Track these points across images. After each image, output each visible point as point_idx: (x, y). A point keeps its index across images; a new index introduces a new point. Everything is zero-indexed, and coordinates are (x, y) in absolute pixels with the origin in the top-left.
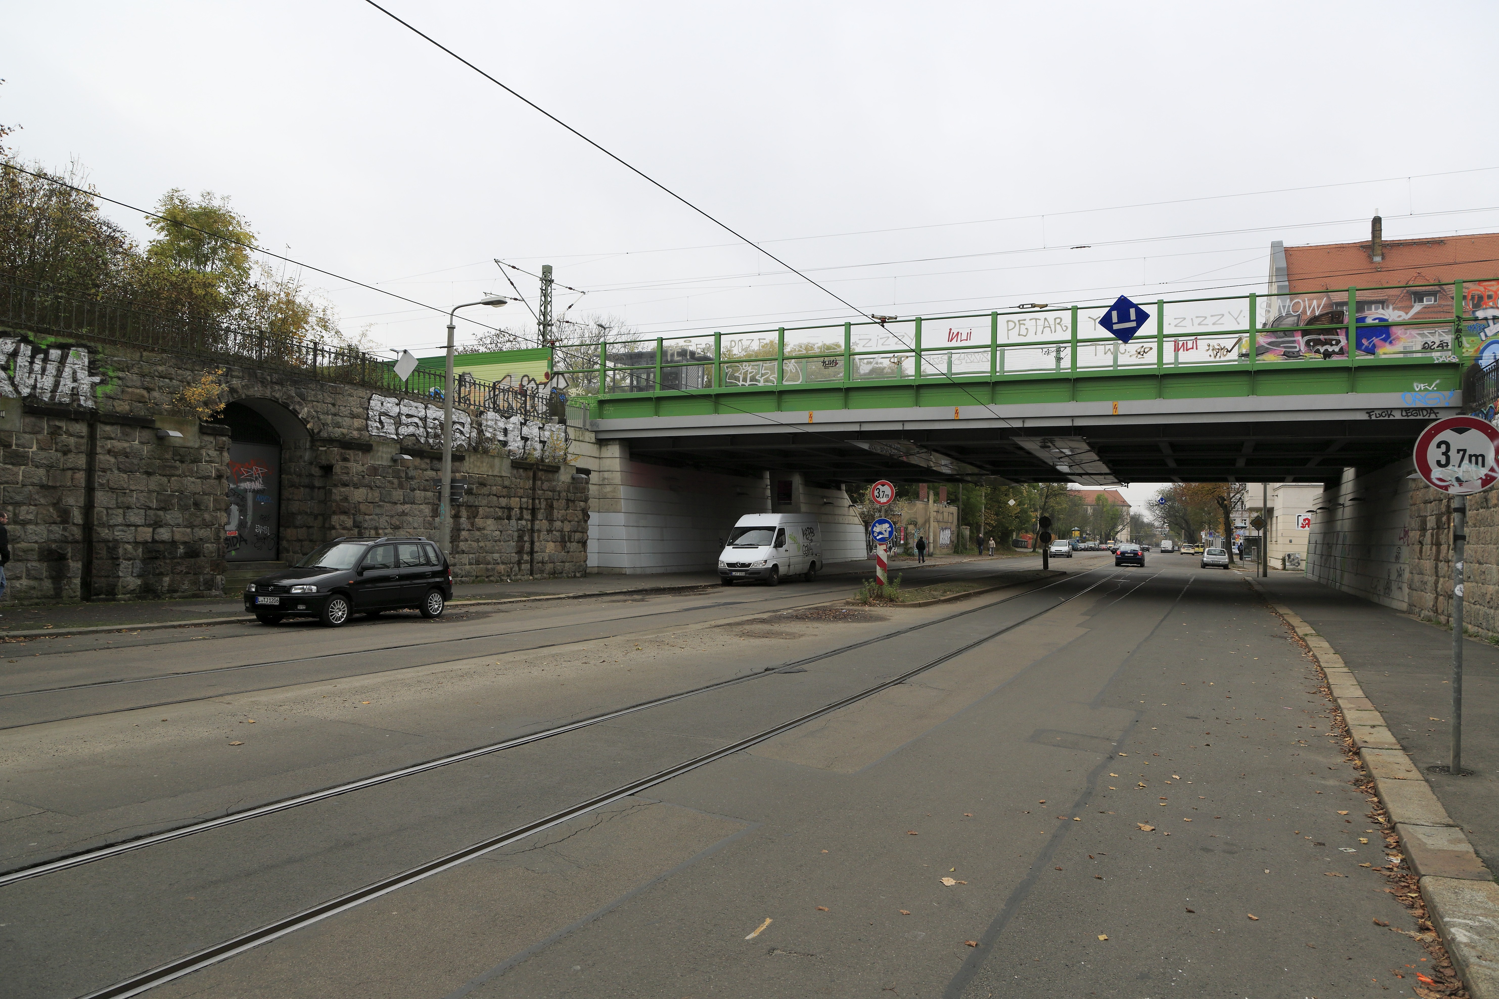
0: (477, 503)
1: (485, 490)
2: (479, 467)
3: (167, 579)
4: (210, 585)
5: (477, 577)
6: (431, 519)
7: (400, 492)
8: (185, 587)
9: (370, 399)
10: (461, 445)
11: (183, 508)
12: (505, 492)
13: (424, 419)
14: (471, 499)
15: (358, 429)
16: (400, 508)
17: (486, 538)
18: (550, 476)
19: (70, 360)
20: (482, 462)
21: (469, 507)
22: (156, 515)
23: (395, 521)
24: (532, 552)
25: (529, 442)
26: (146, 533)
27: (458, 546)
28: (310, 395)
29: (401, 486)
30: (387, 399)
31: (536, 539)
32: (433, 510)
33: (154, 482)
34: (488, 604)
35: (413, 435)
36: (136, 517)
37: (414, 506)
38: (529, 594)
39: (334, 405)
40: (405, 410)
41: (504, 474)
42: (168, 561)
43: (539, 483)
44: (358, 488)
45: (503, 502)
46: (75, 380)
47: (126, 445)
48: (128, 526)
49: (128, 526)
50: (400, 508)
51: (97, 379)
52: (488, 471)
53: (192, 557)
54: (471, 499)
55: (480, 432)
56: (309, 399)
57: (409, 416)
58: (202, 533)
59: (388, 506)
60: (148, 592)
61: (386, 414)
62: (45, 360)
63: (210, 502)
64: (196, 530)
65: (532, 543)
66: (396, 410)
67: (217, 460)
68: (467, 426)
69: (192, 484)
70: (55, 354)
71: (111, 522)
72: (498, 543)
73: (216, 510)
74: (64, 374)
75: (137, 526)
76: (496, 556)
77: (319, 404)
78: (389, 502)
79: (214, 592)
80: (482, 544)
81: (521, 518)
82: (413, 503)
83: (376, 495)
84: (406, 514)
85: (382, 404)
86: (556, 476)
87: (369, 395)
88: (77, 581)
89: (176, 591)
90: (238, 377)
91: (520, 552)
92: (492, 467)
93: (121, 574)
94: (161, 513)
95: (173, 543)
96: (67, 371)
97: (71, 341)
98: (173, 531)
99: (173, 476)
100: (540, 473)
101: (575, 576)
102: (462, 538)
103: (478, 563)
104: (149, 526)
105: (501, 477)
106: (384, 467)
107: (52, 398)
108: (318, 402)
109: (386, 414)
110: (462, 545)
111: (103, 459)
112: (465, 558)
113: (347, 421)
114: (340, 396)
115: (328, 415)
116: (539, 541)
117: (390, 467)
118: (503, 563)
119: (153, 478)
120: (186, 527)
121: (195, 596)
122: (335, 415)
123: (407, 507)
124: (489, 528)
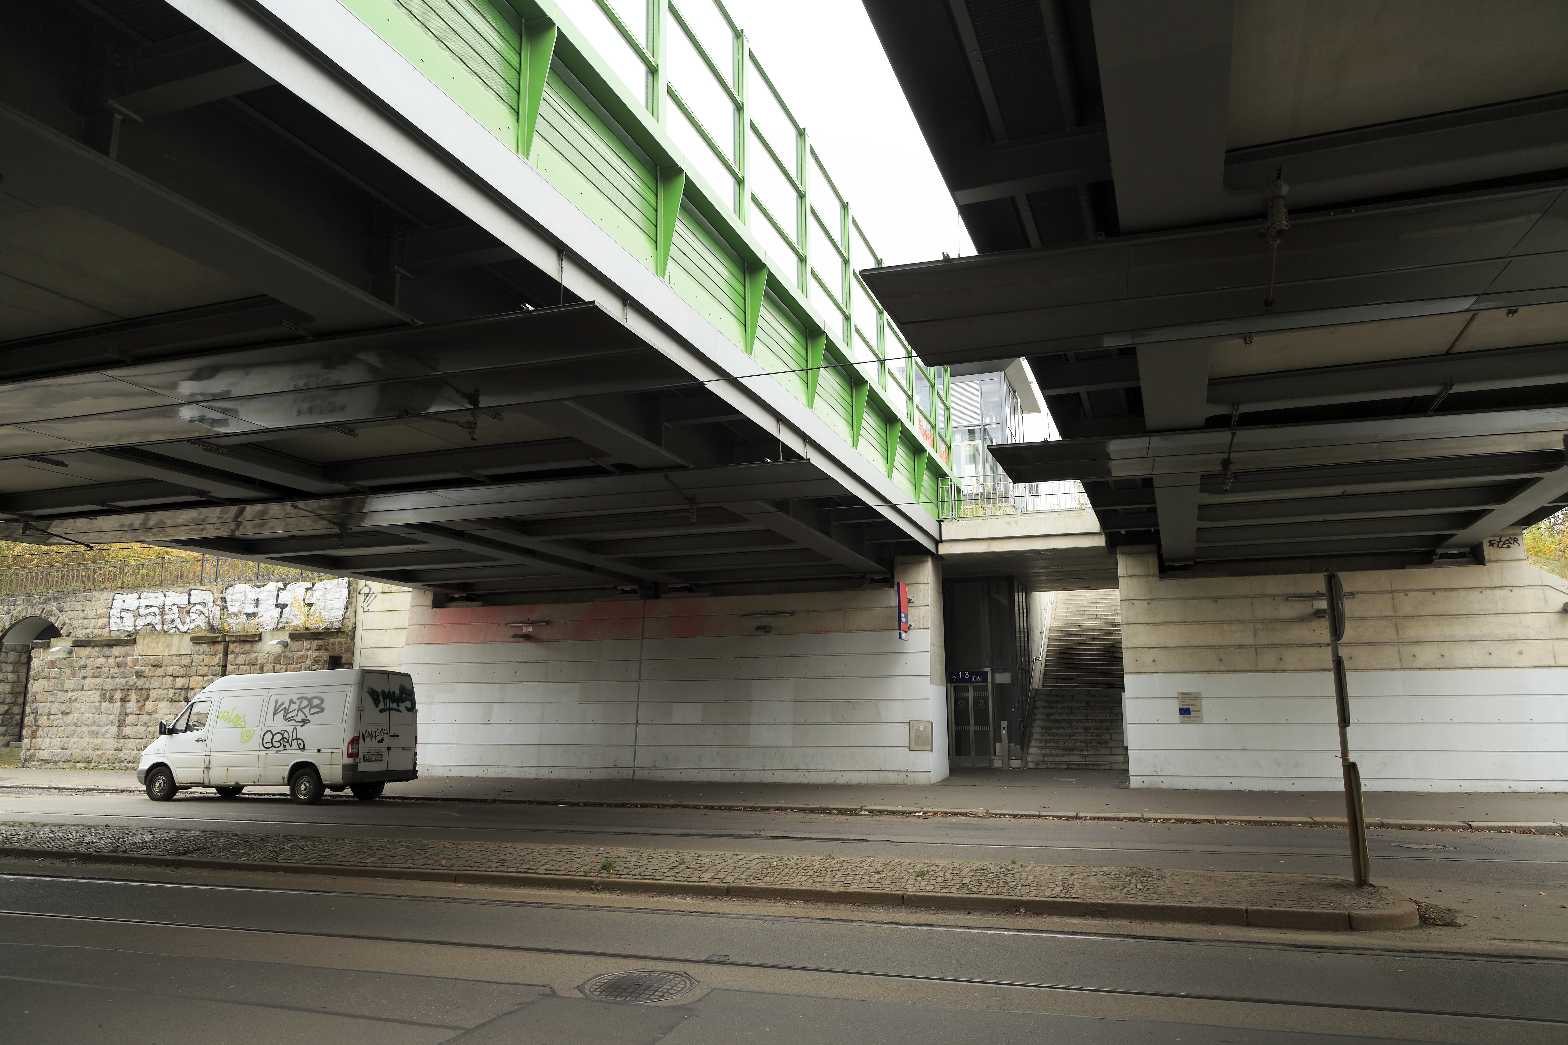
0: (147, 686)
1: (159, 672)
2: (154, 648)
6: (97, 704)
7: (72, 681)
9: (113, 599)
10: (198, 626)
12: (183, 671)
13: (162, 609)
14: (140, 683)
18: (248, 647)
20: (158, 643)
23: (63, 708)
28: (66, 606)
29: (74, 675)
39: (83, 611)
40: (144, 602)
41: (182, 653)
45: (180, 682)
50: (70, 694)
52: (164, 651)
54: (140, 683)
57: (147, 607)
66: (137, 603)
68: (210, 604)
84: (75, 700)
86: (258, 646)
92: (169, 646)
110: (127, 731)
117: (65, 659)
124: (160, 711)
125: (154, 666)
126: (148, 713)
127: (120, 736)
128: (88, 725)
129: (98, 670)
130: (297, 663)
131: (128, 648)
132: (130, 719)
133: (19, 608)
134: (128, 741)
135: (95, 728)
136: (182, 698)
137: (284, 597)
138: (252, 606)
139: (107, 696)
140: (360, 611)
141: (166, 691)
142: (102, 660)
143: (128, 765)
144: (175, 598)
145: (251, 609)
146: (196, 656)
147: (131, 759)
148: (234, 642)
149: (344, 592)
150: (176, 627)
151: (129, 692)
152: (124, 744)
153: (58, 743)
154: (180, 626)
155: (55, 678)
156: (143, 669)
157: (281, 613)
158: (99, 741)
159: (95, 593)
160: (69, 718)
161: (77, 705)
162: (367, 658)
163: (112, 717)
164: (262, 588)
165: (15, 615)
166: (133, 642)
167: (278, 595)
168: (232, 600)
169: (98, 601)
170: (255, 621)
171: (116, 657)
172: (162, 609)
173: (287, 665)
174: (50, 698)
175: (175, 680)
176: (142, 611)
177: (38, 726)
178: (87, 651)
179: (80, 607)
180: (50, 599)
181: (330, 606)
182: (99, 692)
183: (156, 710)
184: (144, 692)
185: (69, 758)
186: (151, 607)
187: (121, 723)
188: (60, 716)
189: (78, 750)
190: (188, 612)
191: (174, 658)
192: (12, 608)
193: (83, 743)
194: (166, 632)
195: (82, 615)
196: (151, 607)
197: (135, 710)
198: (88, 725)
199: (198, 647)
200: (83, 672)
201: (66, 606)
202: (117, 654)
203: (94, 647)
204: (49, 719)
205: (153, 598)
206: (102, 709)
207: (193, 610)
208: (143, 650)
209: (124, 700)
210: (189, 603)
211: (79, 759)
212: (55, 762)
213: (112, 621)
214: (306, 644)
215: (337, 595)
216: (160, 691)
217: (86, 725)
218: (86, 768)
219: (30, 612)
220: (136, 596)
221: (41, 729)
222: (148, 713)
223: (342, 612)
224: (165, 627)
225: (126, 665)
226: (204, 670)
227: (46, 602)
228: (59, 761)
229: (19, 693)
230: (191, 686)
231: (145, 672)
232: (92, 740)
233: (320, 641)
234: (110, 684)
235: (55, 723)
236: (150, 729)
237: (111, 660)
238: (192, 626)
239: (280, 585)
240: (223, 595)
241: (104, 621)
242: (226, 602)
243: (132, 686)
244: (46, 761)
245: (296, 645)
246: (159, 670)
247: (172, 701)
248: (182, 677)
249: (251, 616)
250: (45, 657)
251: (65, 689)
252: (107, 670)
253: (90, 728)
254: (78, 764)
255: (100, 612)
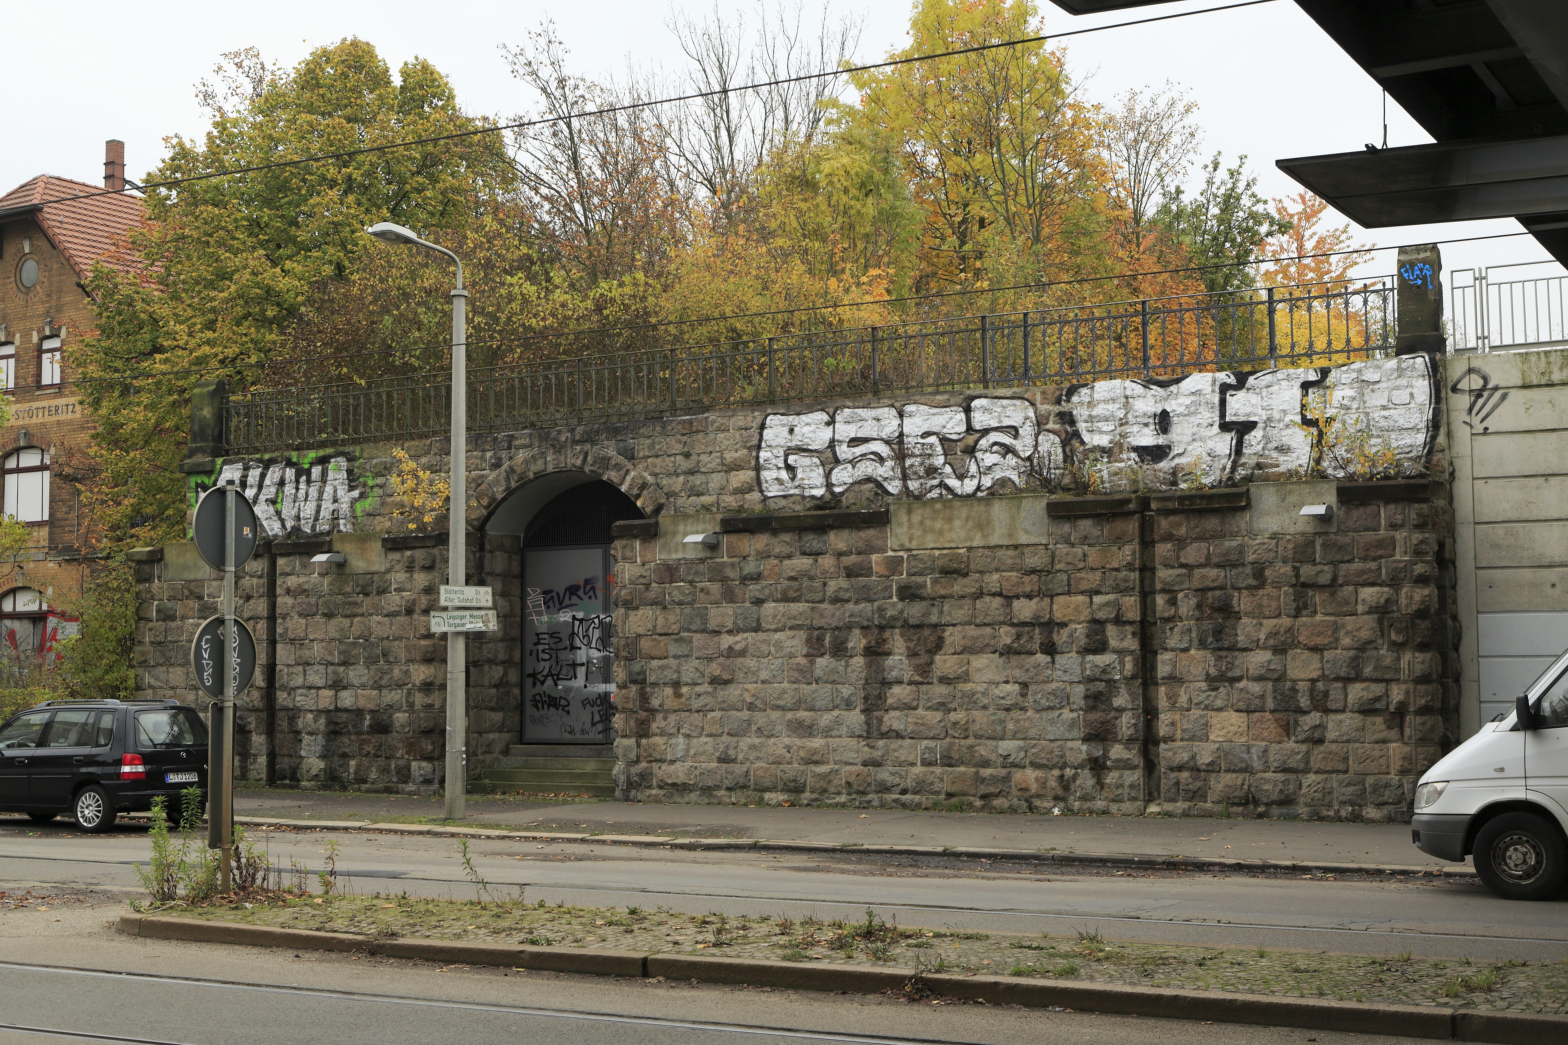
0: (934, 619)
1: (959, 586)
2: (941, 533)
3: (353, 763)
4: (405, 775)
5: (950, 795)
6: (802, 661)
8: (373, 776)
9: (763, 427)
11: (371, 661)
12: (1030, 584)
13: (898, 443)
14: (915, 611)
15: (738, 491)
16: (726, 641)
17: (970, 701)
18: (1212, 523)
19: (331, 475)
20: (950, 520)
21: (911, 628)
22: (335, 673)
23: (715, 669)
24: (1148, 740)
25: (1254, 438)
26: (326, 698)
27: (880, 721)
28: (642, 446)
29: (730, 596)
30: (803, 417)
31: (1162, 702)
32: (808, 641)
33: (334, 627)
34: (913, 859)
35: (869, 480)
36: (316, 677)
37: (761, 635)
38: (604, 827)
39: (687, 455)
40: (845, 431)
41: (1023, 539)
42: (353, 737)
43: (1163, 549)
44: (636, 608)
45: (1024, 609)
46: (335, 501)
47: (302, 579)
48: (310, 688)
49: (310, 688)
50: (726, 641)
51: (356, 493)
52: (972, 539)
53: (381, 732)
54: (915, 611)
55: (1071, 438)
56: (641, 454)
57: (855, 442)
58: (393, 697)
59: (698, 639)
60: (332, 781)
61: (800, 450)
62: (309, 482)
63: (399, 650)
64: (384, 692)
65: (1150, 713)
66: (826, 434)
67: (408, 586)
68: (1027, 431)
69: (379, 625)
70: (316, 471)
71: (292, 684)
72: (1016, 714)
73: (409, 661)
74: (325, 496)
75: (319, 688)
76: (1007, 746)
77: (658, 461)
78: (703, 631)
79: (411, 787)
80: (958, 716)
81: (1097, 646)
82: (757, 629)
83: (672, 619)
84: (743, 653)
85: (791, 431)
86: (1242, 521)
87: (759, 420)
88: (263, 760)
89: (365, 781)
90: (525, 446)
91: (1100, 735)
92: (983, 526)
93: (303, 753)
94: (342, 669)
95: (359, 712)
96: (329, 489)
97: (329, 451)
98: (356, 696)
99: (355, 616)
100: (1164, 524)
101: (1356, 818)
102: (890, 701)
103: (948, 761)
104: (330, 687)
105: (1016, 547)
106: (689, 562)
107: (313, 527)
108: (657, 456)
109: (800, 450)
110: (893, 720)
111: (284, 602)
112: (904, 750)
113: (716, 480)
114: (701, 436)
115: (678, 475)
116: (1173, 706)
117: (702, 560)
118: (1035, 765)
119: (334, 621)
120: (373, 688)
121: (388, 790)
122: (691, 472)
123: (739, 640)
124: (976, 677)
125: (946, 572)
126: (945, 680)
127: (872, 732)
128: (783, 708)
129: (795, 584)
130: (1364, 559)
131: (871, 532)
132: (898, 693)
133: (521, 455)
134: (895, 744)
135: (802, 714)
136: (1036, 646)
137: (1240, 405)
138: (1149, 431)
139: (825, 641)
140: (1462, 433)
141: (988, 630)
142: (802, 563)
143: (908, 797)
144: (927, 421)
145: (1147, 438)
146: (1062, 548)
147: (909, 783)
148: (1168, 513)
149: (1422, 388)
150: (942, 485)
151: (887, 634)
152: (887, 752)
153: (709, 748)
154: (953, 482)
155: (680, 603)
156: (919, 579)
157: (1240, 444)
158: (817, 743)
159: (711, 416)
160: (733, 692)
161: (750, 662)
162: (1496, 546)
163: (846, 691)
164: (1173, 388)
165: (519, 470)
166: (879, 519)
167: (1223, 403)
168: (1091, 419)
169: (724, 435)
170: (1164, 465)
171: (840, 554)
172: (898, 443)
173: (1335, 564)
174: (674, 649)
175: (1010, 605)
176: (844, 452)
177: (653, 711)
178: (761, 541)
179: (678, 448)
180: (597, 432)
181: (1383, 423)
182: (802, 635)
183: (967, 673)
184: (926, 632)
185: (742, 781)
186: (866, 440)
187: (874, 703)
188: (706, 688)
189: (758, 764)
190: (971, 451)
191: (1000, 553)
192: (504, 454)
193: (779, 745)
194: (918, 498)
195: (685, 464)
196: (866, 440)
197: (908, 674)
198: (783, 708)
199: (1067, 527)
200: (754, 589)
201: (642, 446)
202: (842, 546)
203: (775, 532)
204: (678, 695)
205: (877, 422)
206: (818, 672)
207: (984, 443)
208: (903, 535)
209: (875, 652)
210: (970, 429)
211: (767, 783)
212: (707, 790)
213: (766, 475)
214: (1385, 513)
215: (1402, 396)
216: (972, 631)
217: (777, 707)
218: (793, 805)
219: (551, 462)
220: (825, 417)
221: (659, 716)
222: (945, 680)
223: (1421, 438)
224: (913, 485)
225: (869, 572)
226: (1093, 579)
227: (589, 439)
228: (718, 788)
229: (513, 640)
230: (1058, 615)
231: (924, 586)
232: (798, 742)
233: (1425, 506)
234: (832, 615)
235: (696, 704)
236: (953, 716)
237: (827, 562)
238: (987, 482)
239: (1224, 377)
240: (1065, 407)
241: (745, 476)
242: (1072, 422)
243: (893, 618)
244: (681, 788)
245: (1359, 514)
246: (962, 581)
247: (1007, 652)
248: (1029, 597)
249: (1157, 453)
250: (649, 556)
251: (712, 624)
252: (817, 584)
253: (789, 715)
254: (767, 796)
255: (730, 456)
